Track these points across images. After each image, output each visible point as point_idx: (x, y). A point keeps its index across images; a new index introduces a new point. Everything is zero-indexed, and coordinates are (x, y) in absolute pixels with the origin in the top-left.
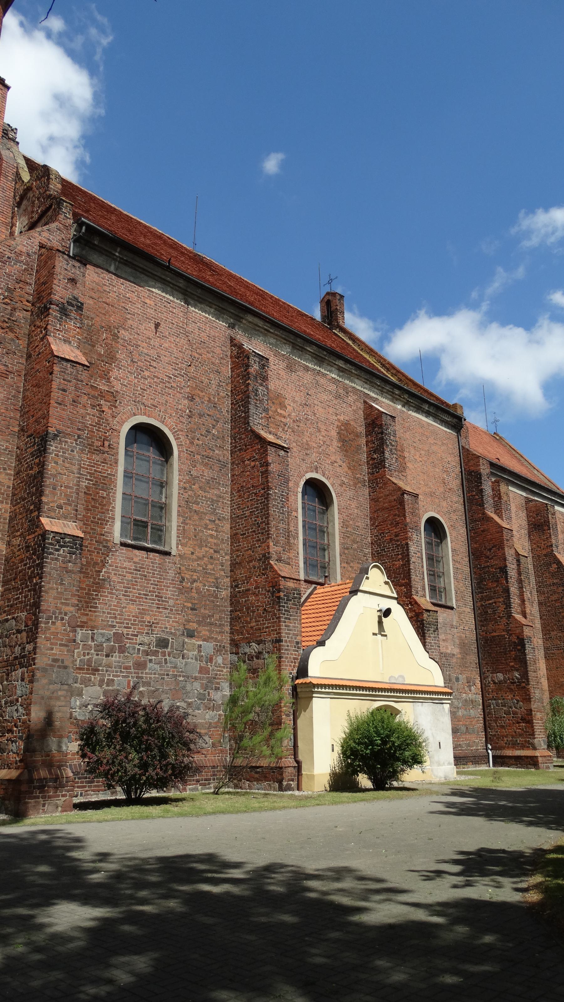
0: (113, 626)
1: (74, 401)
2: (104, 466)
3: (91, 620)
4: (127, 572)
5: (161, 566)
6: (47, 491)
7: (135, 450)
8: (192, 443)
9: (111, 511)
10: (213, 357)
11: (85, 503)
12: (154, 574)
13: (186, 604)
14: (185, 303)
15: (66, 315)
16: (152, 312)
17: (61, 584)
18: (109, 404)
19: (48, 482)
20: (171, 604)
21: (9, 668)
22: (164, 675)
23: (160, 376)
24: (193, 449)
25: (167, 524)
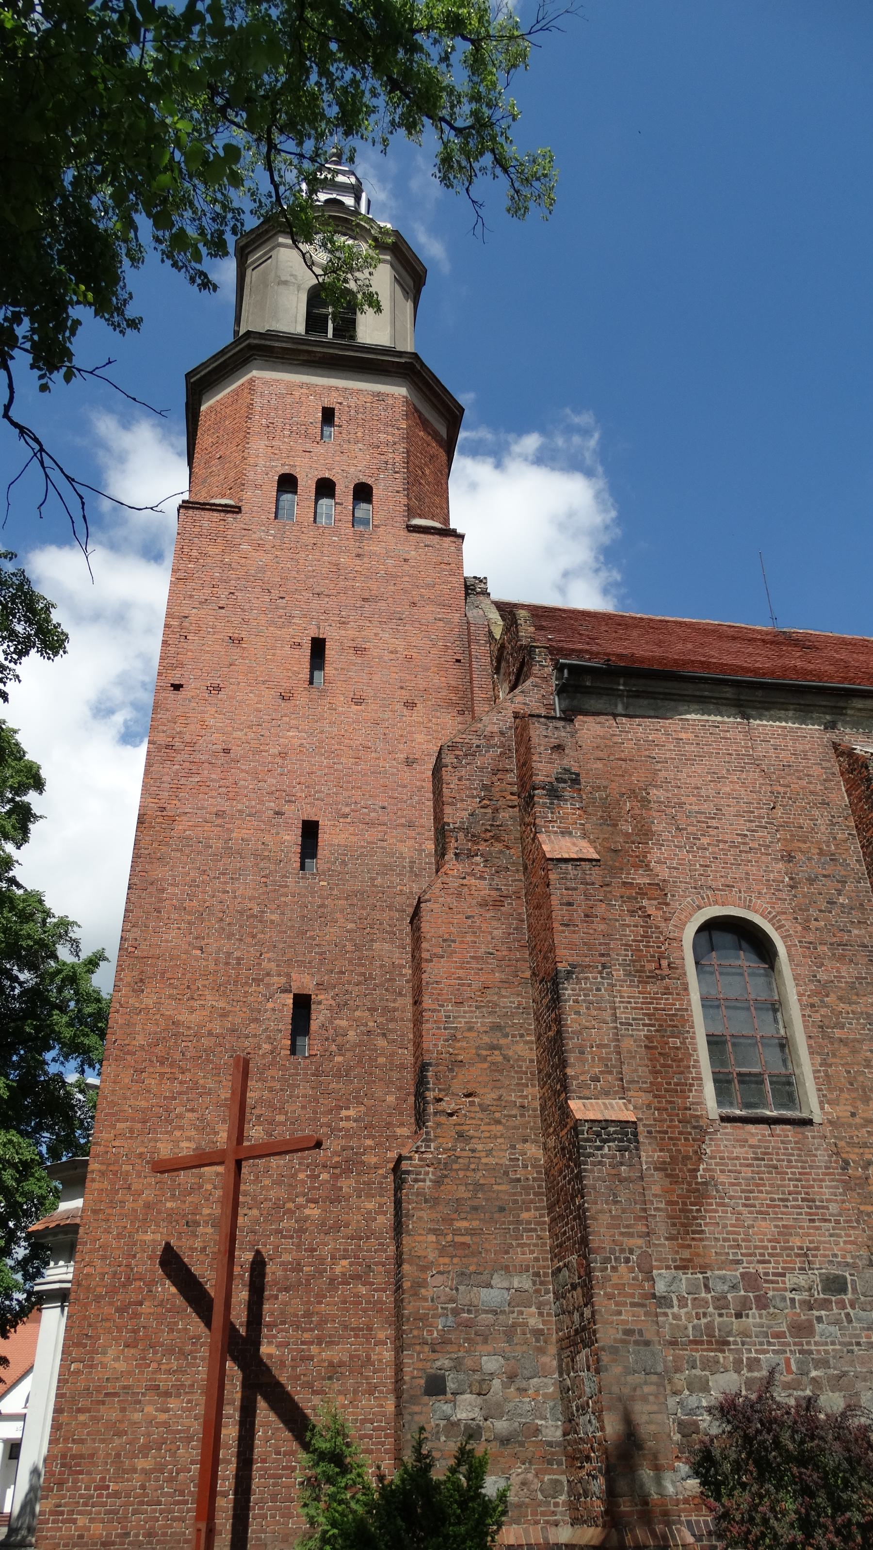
0: (738, 1262)
1: (587, 916)
2: (667, 999)
3: (698, 1255)
4: (741, 1165)
5: (800, 1145)
6: (572, 1058)
7: (715, 961)
8: (807, 928)
9: (694, 1067)
10: (810, 783)
11: (649, 1063)
12: (790, 1161)
13: (862, 1208)
14: (743, 718)
15: (558, 797)
16: (693, 748)
17: (616, 1202)
18: (655, 902)
19: (570, 1044)
20: (835, 1212)
21: (572, 1349)
22: (851, 1344)
23: (727, 837)
24: (811, 937)
25: (797, 1072)
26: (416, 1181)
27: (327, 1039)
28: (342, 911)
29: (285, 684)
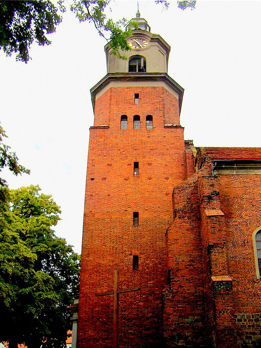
1: (219, 230)
15: (212, 199)
26: (167, 297)
27: (144, 266)
28: (147, 235)
29: (126, 176)
